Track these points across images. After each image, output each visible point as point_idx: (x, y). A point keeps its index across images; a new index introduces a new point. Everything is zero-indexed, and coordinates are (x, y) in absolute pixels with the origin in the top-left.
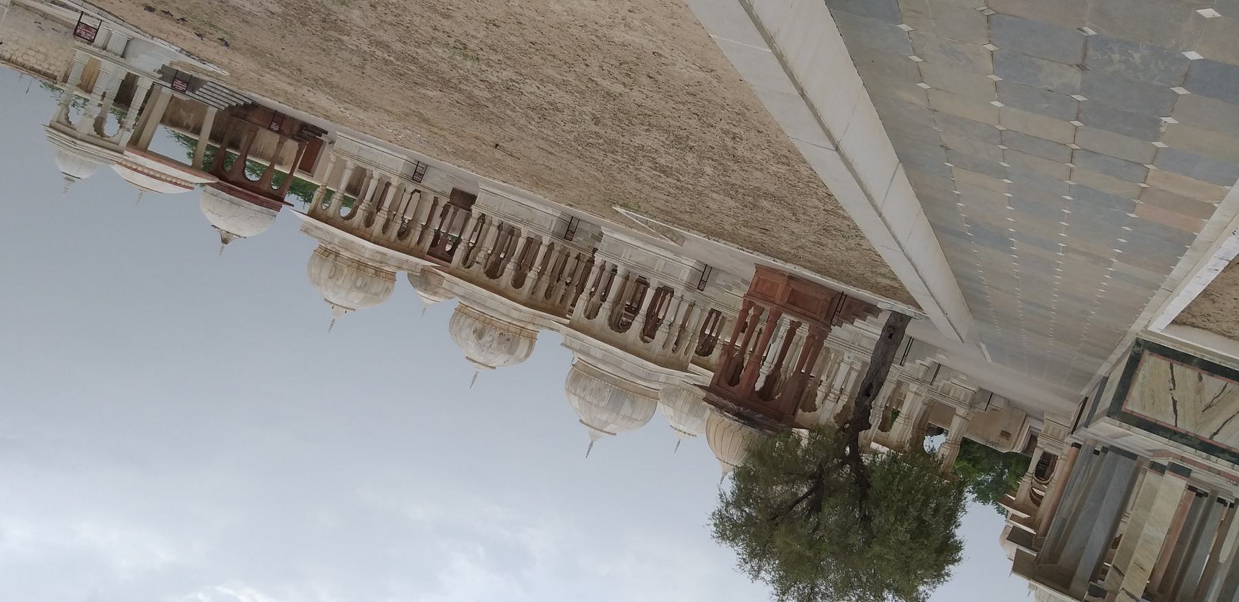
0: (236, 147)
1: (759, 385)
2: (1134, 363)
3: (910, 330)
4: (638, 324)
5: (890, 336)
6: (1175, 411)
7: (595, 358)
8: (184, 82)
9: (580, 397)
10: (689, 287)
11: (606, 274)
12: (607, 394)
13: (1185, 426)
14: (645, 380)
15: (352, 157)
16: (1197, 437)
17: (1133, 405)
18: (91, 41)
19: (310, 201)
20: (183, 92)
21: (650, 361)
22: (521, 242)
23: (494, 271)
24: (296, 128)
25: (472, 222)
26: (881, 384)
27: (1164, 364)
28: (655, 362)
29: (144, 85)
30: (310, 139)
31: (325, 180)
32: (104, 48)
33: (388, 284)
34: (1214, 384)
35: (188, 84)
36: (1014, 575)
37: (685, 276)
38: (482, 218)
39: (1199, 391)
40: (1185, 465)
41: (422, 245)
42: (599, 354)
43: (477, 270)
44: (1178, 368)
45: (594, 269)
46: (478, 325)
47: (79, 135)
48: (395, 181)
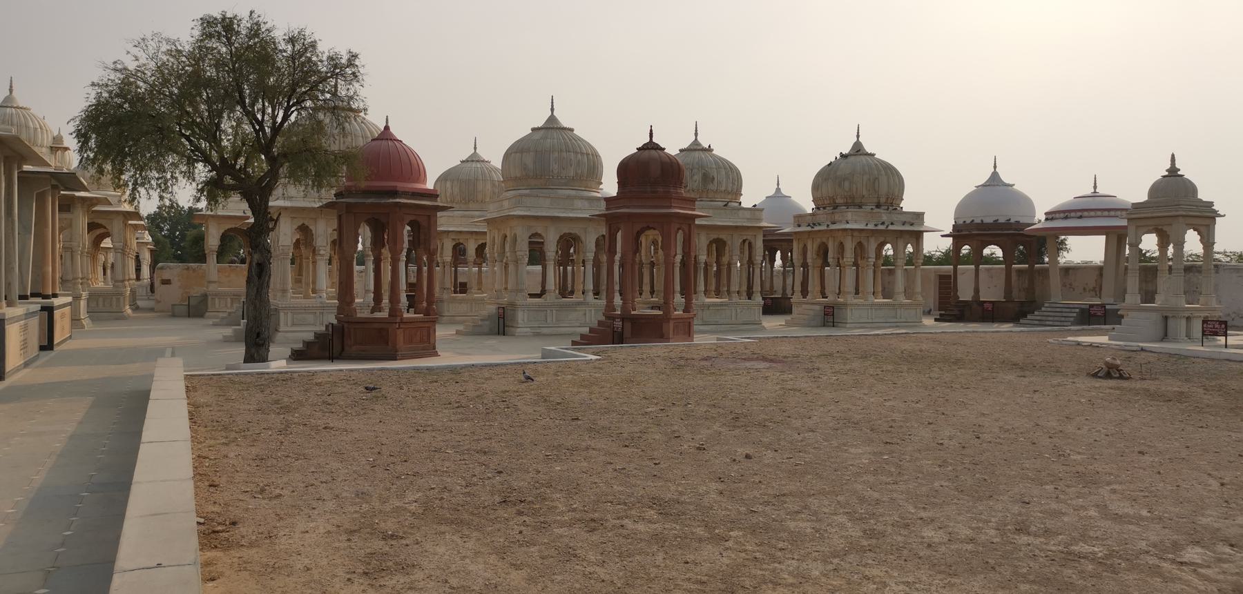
0: (1019, 271)
1: (778, 254)
3: (240, 350)
4: (551, 250)
5: (258, 335)
7: (582, 198)
8: (1095, 315)
9: (582, 154)
12: (555, 167)
14: (521, 196)
15: (901, 305)
18: (1204, 322)
19: (212, 199)
20: (1091, 306)
23: (823, 252)
25: (757, 287)
29: (1133, 298)
30: (574, 343)
31: (919, 274)
32: (1188, 319)
35: (1090, 315)
37: (521, 316)
38: (750, 295)
41: (801, 246)
42: (578, 204)
43: (734, 243)
46: (712, 187)
47: (1181, 219)
48: (851, 299)
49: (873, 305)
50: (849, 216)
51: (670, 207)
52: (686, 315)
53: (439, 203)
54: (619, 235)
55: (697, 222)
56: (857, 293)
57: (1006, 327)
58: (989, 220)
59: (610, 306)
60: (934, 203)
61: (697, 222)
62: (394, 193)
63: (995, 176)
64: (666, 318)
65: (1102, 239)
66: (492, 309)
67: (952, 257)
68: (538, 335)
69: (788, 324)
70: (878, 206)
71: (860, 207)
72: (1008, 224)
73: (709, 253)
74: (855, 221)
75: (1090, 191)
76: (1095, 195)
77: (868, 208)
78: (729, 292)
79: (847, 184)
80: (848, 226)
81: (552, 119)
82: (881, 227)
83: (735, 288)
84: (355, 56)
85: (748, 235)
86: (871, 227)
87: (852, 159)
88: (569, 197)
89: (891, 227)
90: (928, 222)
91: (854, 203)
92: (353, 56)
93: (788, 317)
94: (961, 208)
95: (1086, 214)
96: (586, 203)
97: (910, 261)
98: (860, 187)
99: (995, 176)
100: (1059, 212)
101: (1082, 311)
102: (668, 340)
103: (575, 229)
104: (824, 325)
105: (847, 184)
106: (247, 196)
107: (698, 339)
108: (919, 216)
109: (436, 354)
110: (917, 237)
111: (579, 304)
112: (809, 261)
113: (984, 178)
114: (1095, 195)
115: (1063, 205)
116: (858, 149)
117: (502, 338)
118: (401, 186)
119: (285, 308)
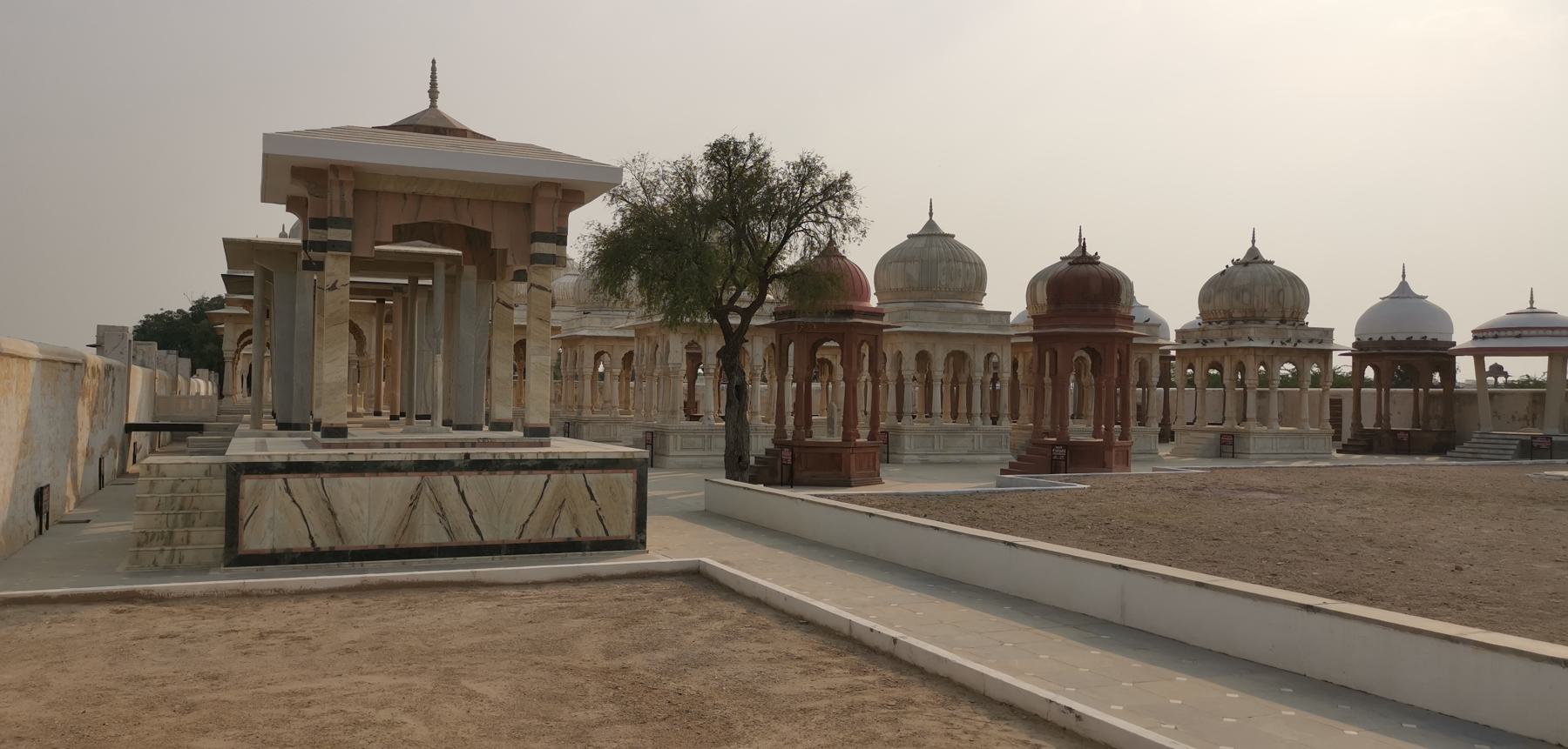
2: (641, 524)
4: (939, 370)
5: (740, 459)
10: (898, 431)
11: (963, 409)
13: (576, 477)
15: (1310, 434)
16: (562, 471)
20: (1534, 437)
27: (614, 533)
28: (584, 337)
31: (1306, 396)
33: (1210, 307)
34: (564, 532)
36: (1069, 248)
37: (908, 442)
39: (574, 518)
40: (537, 439)
42: (968, 318)
44: (600, 533)
45: (1007, 411)
48: (1253, 426)
49: (1278, 433)
50: (1252, 332)
54: (792, 348)
55: (1135, 341)
56: (428, 417)
57: (1432, 460)
58: (1401, 337)
60: (1338, 312)
61: (1135, 341)
62: (850, 313)
63: (1404, 286)
64: (1108, 445)
65: (1546, 359)
68: (926, 463)
70: (1283, 321)
71: (1262, 322)
72: (1424, 342)
73: (946, 371)
75: (1525, 306)
76: (1532, 311)
77: (1272, 323)
78: (970, 415)
79: (1246, 296)
80: (1252, 344)
81: (931, 224)
82: (1289, 345)
83: (977, 409)
86: (1277, 345)
87: (1250, 267)
88: (957, 311)
89: (1299, 346)
91: (1253, 317)
92: (847, 177)
94: (1363, 323)
95: (1525, 332)
97: (1316, 381)
98: (1254, 298)
99: (1404, 286)
100: (1492, 330)
101: (1522, 442)
104: (1221, 455)
105: (1246, 296)
107: (1136, 470)
108: (1328, 333)
110: (1326, 355)
112: (1020, 378)
113: (1391, 287)
114: (1532, 311)
115: (1495, 321)
116: (1253, 256)
119: (673, 432)
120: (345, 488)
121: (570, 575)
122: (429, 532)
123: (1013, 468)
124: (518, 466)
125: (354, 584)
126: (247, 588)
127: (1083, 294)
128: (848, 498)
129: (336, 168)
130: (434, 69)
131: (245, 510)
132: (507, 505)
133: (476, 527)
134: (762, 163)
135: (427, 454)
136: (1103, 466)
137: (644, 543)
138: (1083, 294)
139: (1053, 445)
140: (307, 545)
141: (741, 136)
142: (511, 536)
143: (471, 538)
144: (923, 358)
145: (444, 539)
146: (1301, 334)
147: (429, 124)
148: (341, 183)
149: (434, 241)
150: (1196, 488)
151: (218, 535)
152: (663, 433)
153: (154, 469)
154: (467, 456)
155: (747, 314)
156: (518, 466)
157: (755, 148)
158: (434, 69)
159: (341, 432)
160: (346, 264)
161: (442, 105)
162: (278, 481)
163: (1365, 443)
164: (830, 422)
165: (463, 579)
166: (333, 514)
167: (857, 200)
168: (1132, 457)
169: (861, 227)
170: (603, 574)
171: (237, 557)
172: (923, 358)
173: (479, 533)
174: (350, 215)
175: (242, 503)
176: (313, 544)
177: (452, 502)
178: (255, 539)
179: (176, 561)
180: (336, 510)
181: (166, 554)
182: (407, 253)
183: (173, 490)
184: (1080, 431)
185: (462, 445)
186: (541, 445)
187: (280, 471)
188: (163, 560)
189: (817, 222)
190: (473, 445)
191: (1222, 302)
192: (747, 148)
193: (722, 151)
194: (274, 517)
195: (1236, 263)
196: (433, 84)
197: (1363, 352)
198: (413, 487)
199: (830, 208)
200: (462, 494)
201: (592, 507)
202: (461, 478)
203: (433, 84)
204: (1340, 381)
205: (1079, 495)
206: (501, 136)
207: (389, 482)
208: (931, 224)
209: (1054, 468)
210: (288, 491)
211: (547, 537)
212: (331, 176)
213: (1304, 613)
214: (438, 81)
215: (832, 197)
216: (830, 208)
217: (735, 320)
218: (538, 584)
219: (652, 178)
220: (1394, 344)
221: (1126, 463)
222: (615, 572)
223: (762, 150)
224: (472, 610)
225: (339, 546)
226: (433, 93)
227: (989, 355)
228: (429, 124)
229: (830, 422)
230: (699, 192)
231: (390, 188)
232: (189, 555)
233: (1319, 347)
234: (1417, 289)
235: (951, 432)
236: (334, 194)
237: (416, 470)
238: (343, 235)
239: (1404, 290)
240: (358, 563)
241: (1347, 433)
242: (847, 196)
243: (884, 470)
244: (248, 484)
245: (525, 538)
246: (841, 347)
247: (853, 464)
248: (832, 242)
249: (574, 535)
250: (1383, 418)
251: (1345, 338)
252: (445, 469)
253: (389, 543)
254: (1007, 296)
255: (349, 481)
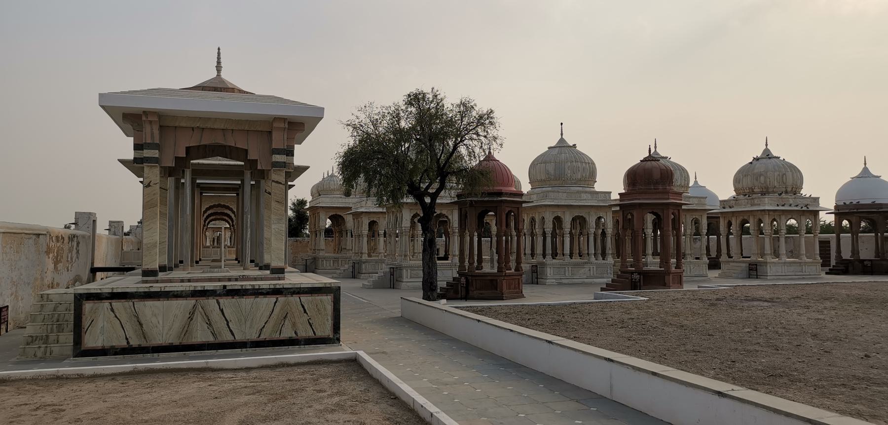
2: (336, 328)
6: (303, 307)
7: (586, 192)
10: (543, 265)
12: (569, 173)
13: (295, 299)
15: (806, 263)
17: (328, 299)
21: (549, 206)
22: (783, 250)
24: (850, 268)
26: (424, 251)
27: (319, 334)
28: (362, 212)
31: (803, 240)
37: (549, 271)
38: (604, 255)
39: (294, 325)
40: (276, 275)
41: (726, 222)
42: (584, 196)
44: (311, 334)
48: (769, 259)
51: (668, 199)
52: (678, 270)
53: (524, 199)
55: (684, 207)
59: (624, 263)
60: (824, 188)
62: (500, 194)
63: (866, 170)
64: (668, 272)
66: (385, 268)
67: (837, 229)
68: (560, 284)
69: (720, 276)
74: (768, 204)
81: (562, 140)
84: (492, 112)
85: (696, 215)
88: (578, 192)
90: (822, 204)
93: (719, 271)
96: (589, 195)
99: (866, 170)
102: (669, 287)
103: (583, 213)
104: (749, 277)
105: (762, 178)
106: (415, 197)
107: (686, 287)
108: (816, 200)
109: (523, 296)
110: (815, 213)
111: (586, 263)
116: (767, 154)
117: (392, 290)
118: (505, 189)
119: (406, 267)
120: (148, 308)
121: (270, 363)
122: (201, 335)
123: (609, 287)
124: (257, 293)
125: (128, 370)
126: (60, 374)
127: (653, 180)
128: (468, 309)
129: (146, 113)
130: (219, 54)
131: (86, 323)
132: (252, 317)
133: (231, 331)
134: (439, 106)
135: (199, 286)
136: (665, 285)
137: (339, 340)
138: (653, 180)
139: (632, 273)
140: (124, 343)
141: (427, 89)
142: (254, 337)
143: (229, 338)
144: (558, 220)
145: (211, 339)
146: (798, 201)
147: (217, 87)
148: (151, 122)
149: (226, 156)
150: (718, 299)
151: (67, 338)
152: (400, 268)
153: (45, 296)
154: (225, 287)
155: (434, 196)
156: (257, 293)
157: (442, 100)
158: (219, 54)
159: (281, 271)
160: (157, 171)
161: (223, 75)
162: (106, 304)
163: (845, 268)
164: (492, 260)
165: (200, 366)
166: (141, 324)
167: (497, 125)
168: (684, 279)
169: (498, 141)
170: (292, 362)
171: (81, 352)
172: (558, 220)
173: (233, 335)
174: (157, 141)
175: (84, 318)
176: (128, 343)
177: (216, 316)
178: (91, 341)
179: (48, 354)
180: (143, 322)
181: (42, 349)
182: (203, 164)
183: (54, 310)
184: (652, 263)
185: (219, 280)
186: (279, 279)
187: (107, 298)
188: (40, 354)
189: (471, 139)
190: (230, 280)
191: (747, 182)
192: (430, 96)
193: (415, 99)
194: (103, 327)
195: (757, 159)
196: (219, 63)
197: (840, 212)
198: (191, 306)
199: (480, 130)
200: (222, 311)
201: (306, 317)
202: (221, 301)
203: (219, 63)
204: (826, 229)
205: (637, 305)
206: (258, 91)
207: (181, 302)
208: (562, 140)
209: (634, 286)
210: (112, 310)
211: (276, 336)
212: (144, 118)
213: (717, 397)
214: (222, 60)
215: (483, 124)
216: (480, 130)
217: (428, 200)
218: (248, 369)
219: (376, 117)
220: (859, 206)
221: (680, 283)
222: (300, 361)
223: (439, 97)
224: (190, 388)
225: (144, 344)
226: (219, 68)
227: (599, 218)
228: (217, 87)
229: (492, 260)
230: (403, 124)
231: (183, 124)
232: (56, 349)
233: (810, 211)
234: (874, 171)
235: (577, 265)
236: (147, 128)
237: (192, 296)
238: (155, 153)
239: (866, 173)
240: (156, 355)
241: (833, 262)
242: (491, 123)
243: (526, 290)
244: (88, 306)
245: (262, 337)
246: (496, 215)
247: (505, 285)
248: (490, 153)
249: (294, 335)
250: (855, 251)
251: (828, 202)
252: (211, 295)
253: (176, 342)
254: (611, 183)
255: (150, 303)
